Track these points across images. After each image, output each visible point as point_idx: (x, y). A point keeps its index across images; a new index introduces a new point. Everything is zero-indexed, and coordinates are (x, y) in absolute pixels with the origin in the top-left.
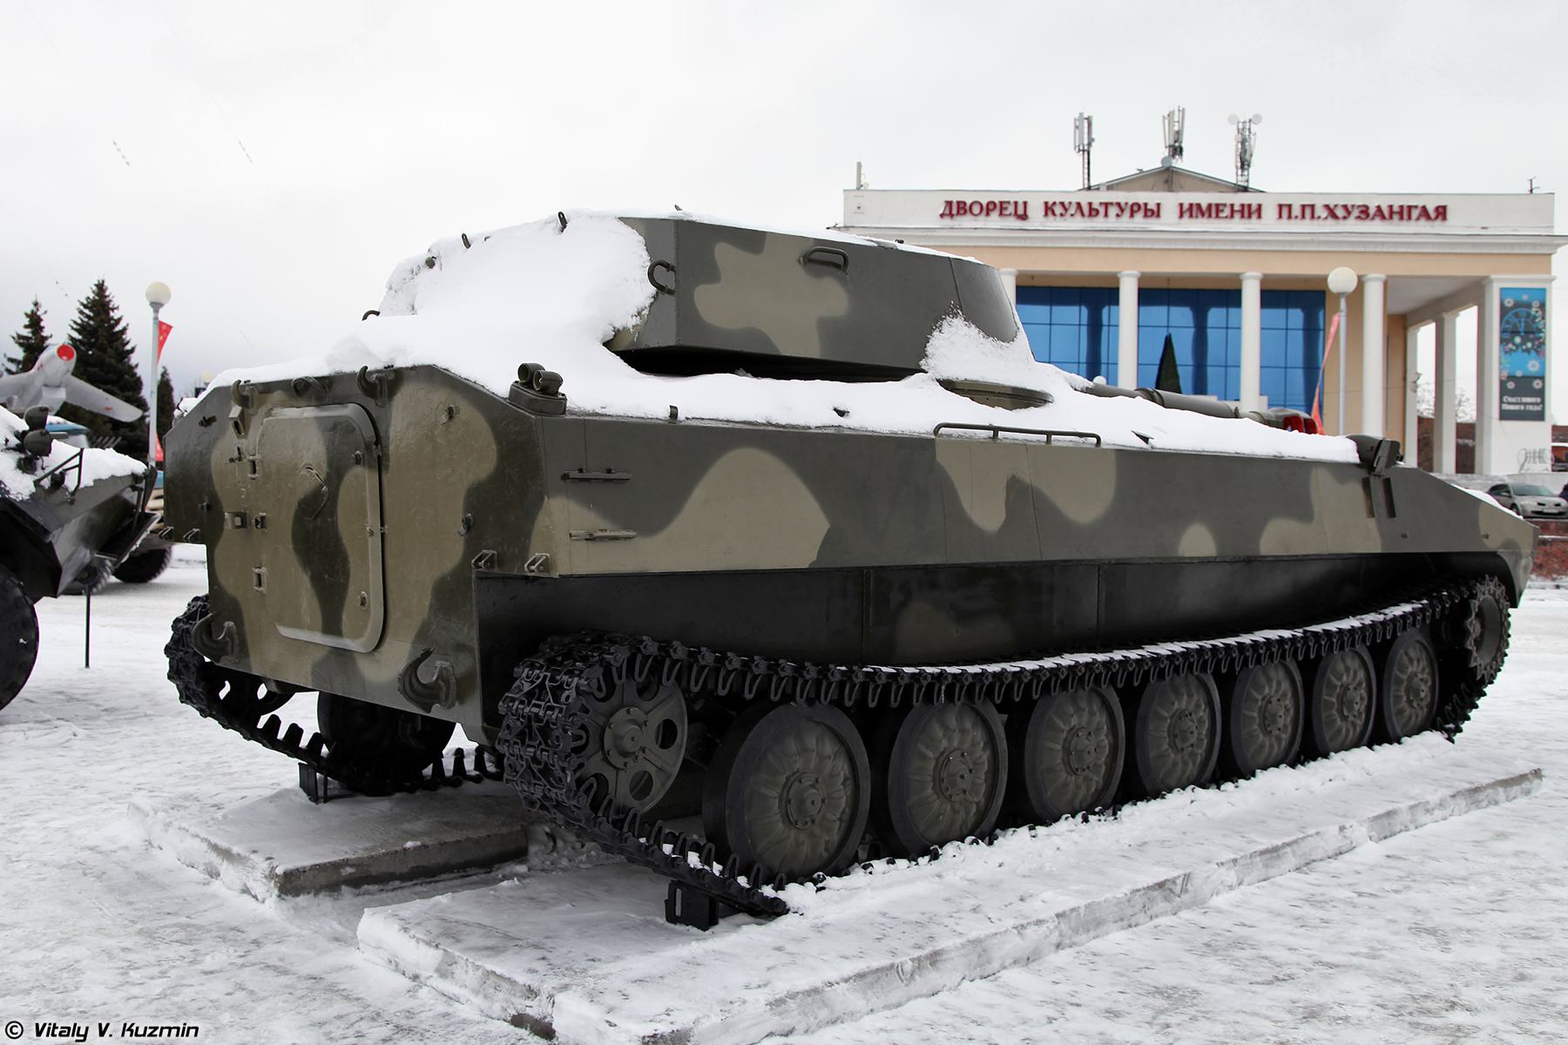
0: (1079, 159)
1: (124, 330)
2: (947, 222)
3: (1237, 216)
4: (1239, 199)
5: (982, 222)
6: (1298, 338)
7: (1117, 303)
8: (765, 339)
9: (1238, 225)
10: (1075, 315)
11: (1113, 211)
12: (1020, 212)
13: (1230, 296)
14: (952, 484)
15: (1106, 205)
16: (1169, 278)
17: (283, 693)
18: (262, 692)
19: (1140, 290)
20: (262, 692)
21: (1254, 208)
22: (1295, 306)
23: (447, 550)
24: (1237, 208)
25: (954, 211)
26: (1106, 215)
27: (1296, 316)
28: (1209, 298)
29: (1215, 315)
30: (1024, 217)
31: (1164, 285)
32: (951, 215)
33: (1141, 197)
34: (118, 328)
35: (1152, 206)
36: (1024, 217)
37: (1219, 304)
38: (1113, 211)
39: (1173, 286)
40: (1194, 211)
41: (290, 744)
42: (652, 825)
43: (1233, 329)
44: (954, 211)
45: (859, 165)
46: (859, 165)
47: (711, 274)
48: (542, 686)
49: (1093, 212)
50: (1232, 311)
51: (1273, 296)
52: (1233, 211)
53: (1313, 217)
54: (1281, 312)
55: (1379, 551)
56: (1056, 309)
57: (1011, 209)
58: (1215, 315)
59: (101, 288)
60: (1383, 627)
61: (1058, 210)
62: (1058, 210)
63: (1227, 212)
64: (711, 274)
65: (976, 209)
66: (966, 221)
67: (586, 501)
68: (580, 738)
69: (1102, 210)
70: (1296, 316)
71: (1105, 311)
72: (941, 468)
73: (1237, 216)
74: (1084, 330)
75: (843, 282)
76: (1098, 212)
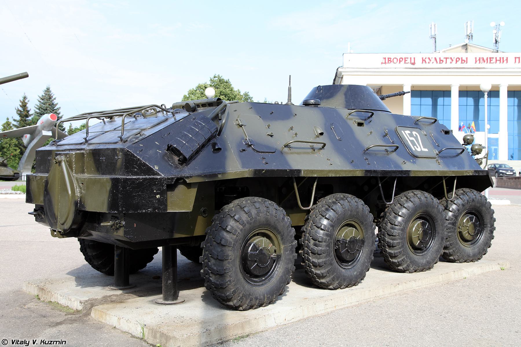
1: (58, 109)
2: (384, 66)
5: (398, 65)
6: (471, 109)
11: (449, 61)
12: (413, 62)
19: (459, 91)
21: (478, 62)
22: (470, 97)
25: (387, 62)
27: (471, 101)
29: (440, 100)
30: (414, 64)
32: (385, 63)
34: (56, 108)
35: (464, 59)
36: (414, 64)
38: (449, 61)
39: (468, 90)
40: (481, 60)
42: (277, 256)
44: (387, 62)
45: (290, 76)
46: (290, 76)
51: (464, 93)
54: (465, 99)
56: (423, 99)
57: (409, 60)
58: (440, 100)
59: (48, 90)
61: (427, 60)
62: (427, 60)
65: (395, 60)
66: (391, 65)
69: (445, 60)
70: (471, 101)
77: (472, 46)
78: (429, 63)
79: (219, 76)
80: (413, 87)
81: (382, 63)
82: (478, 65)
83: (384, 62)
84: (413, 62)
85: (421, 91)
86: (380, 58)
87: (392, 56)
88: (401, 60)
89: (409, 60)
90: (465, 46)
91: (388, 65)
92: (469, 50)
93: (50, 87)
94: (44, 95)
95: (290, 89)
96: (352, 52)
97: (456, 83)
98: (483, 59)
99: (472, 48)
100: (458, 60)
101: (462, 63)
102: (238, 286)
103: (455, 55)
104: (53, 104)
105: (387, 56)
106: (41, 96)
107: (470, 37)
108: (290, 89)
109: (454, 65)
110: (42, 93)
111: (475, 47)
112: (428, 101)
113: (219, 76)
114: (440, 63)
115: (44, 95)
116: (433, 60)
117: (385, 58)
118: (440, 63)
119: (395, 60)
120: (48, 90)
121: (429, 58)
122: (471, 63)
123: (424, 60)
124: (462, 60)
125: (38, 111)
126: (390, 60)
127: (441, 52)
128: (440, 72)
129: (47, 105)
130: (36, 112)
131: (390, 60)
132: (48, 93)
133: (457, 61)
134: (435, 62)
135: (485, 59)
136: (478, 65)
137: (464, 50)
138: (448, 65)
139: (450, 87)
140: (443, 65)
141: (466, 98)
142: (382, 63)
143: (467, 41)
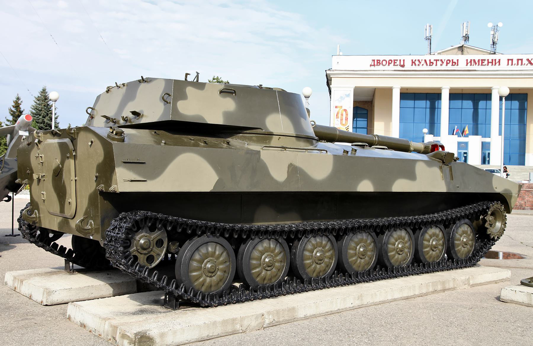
0: (428, 42)
3: (490, 64)
4: (491, 57)
5: (387, 67)
7: (441, 99)
8: (203, 119)
9: (490, 67)
10: (423, 104)
11: (439, 63)
12: (402, 64)
13: (486, 96)
14: (267, 166)
15: (437, 60)
16: (462, 89)
17: (58, 235)
18: (51, 235)
19: (450, 94)
20: (51, 235)
21: (469, 64)
23: (90, 186)
24: (490, 61)
25: (376, 64)
26: (436, 65)
28: (482, 96)
29: (482, 104)
30: (403, 66)
31: (460, 92)
32: (374, 65)
33: (450, 57)
35: (455, 61)
36: (403, 66)
37: (483, 100)
38: (439, 63)
39: (464, 92)
40: (472, 62)
41: (61, 252)
43: (488, 109)
44: (376, 64)
47: (184, 97)
48: (116, 227)
49: (431, 63)
50: (488, 102)
51: (455, 95)
52: (488, 62)
53: (482, 65)
55: (445, 191)
56: (416, 102)
57: (398, 63)
59: (44, 91)
60: (462, 220)
61: (417, 63)
63: (486, 62)
64: (184, 97)
65: (384, 63)
66: (381, 67)
67: (129, 169)
68: (128, 243)
69: (435, 62)
71: (437, 102)
72: (262, 160)
73: (490, 64)
74: (428, 110)
75: (233, 99)
76: (433, 63)
77: (468, 48)
78: (418, 65)
79: (218, 78)
80: (402, 89)
81: (371, 65)
82: (469, 67)
83: (373, 64)
84: (402, 64)
85: (487, 94)
86: (368, 60)
87: (381, 58)
88: (390, 62)
89: (398, 63)
90: (461, 49)
91: (377, 68)
92: (465, 52)
93: (46, 88)
94: (40, 96)
95: (330, 94)
96: (341, 54)
97: (446, 86)
98: (474, 60)
99: (468, 50)
100: (448, 62)
101: (452, 65)
102: (152, 253)
103: (445, 57)
104: (48, 105)
105: (376, 58)
106: (37, 96)
107: (466, 38)
108: (330, 94)
109: (444, 67)
110: (37, 94)
111: (471, 48)
112: (468, 104)
113: (218, 78)
114: (430, 65)
115: (40, 96)
116: (423, 62)
117: (374, 61)
118: (430, 65)
119: (384, 63)
120: (44, 91)
121: (419, 60)
122: (462, 65)
123: (413, 63)
124: (453, 62)
125: (34, 111)
126: (379, 62)
127: (436, 54)
128: (429, 75)
129: (43, 106)
130: (32, 113)
131: (379, 62)
132: (43, 94)
133: (447, 63)
134: (425, 64)
135: (477, 61)
136: (469, 67)
137: (460, 52)
138: (439, 67)
139: (440, 89)
140: (433, 67)
141: (461, 101)
142: (371, 65)
143: (462, 43)
